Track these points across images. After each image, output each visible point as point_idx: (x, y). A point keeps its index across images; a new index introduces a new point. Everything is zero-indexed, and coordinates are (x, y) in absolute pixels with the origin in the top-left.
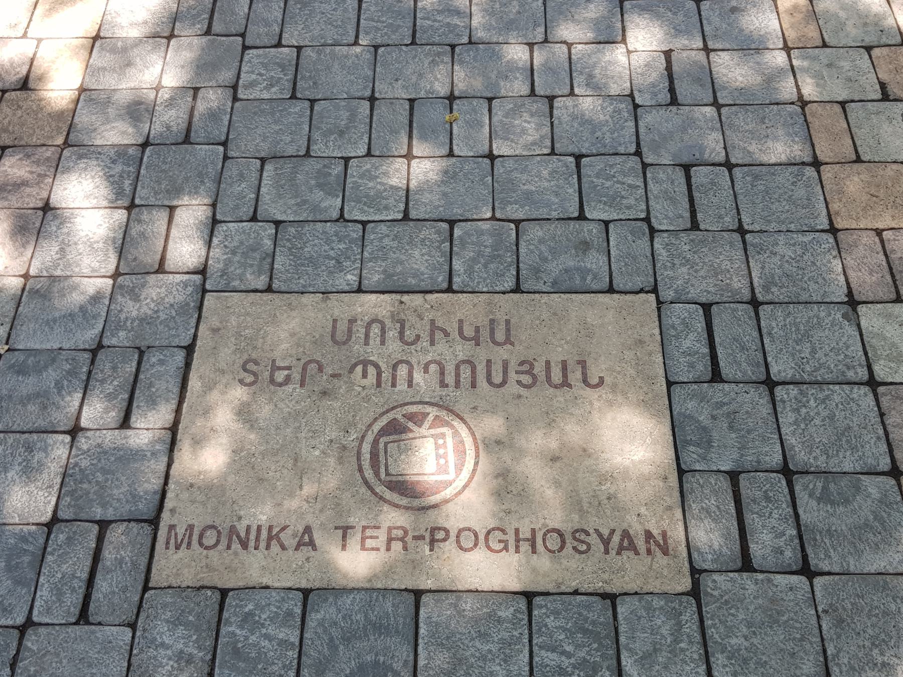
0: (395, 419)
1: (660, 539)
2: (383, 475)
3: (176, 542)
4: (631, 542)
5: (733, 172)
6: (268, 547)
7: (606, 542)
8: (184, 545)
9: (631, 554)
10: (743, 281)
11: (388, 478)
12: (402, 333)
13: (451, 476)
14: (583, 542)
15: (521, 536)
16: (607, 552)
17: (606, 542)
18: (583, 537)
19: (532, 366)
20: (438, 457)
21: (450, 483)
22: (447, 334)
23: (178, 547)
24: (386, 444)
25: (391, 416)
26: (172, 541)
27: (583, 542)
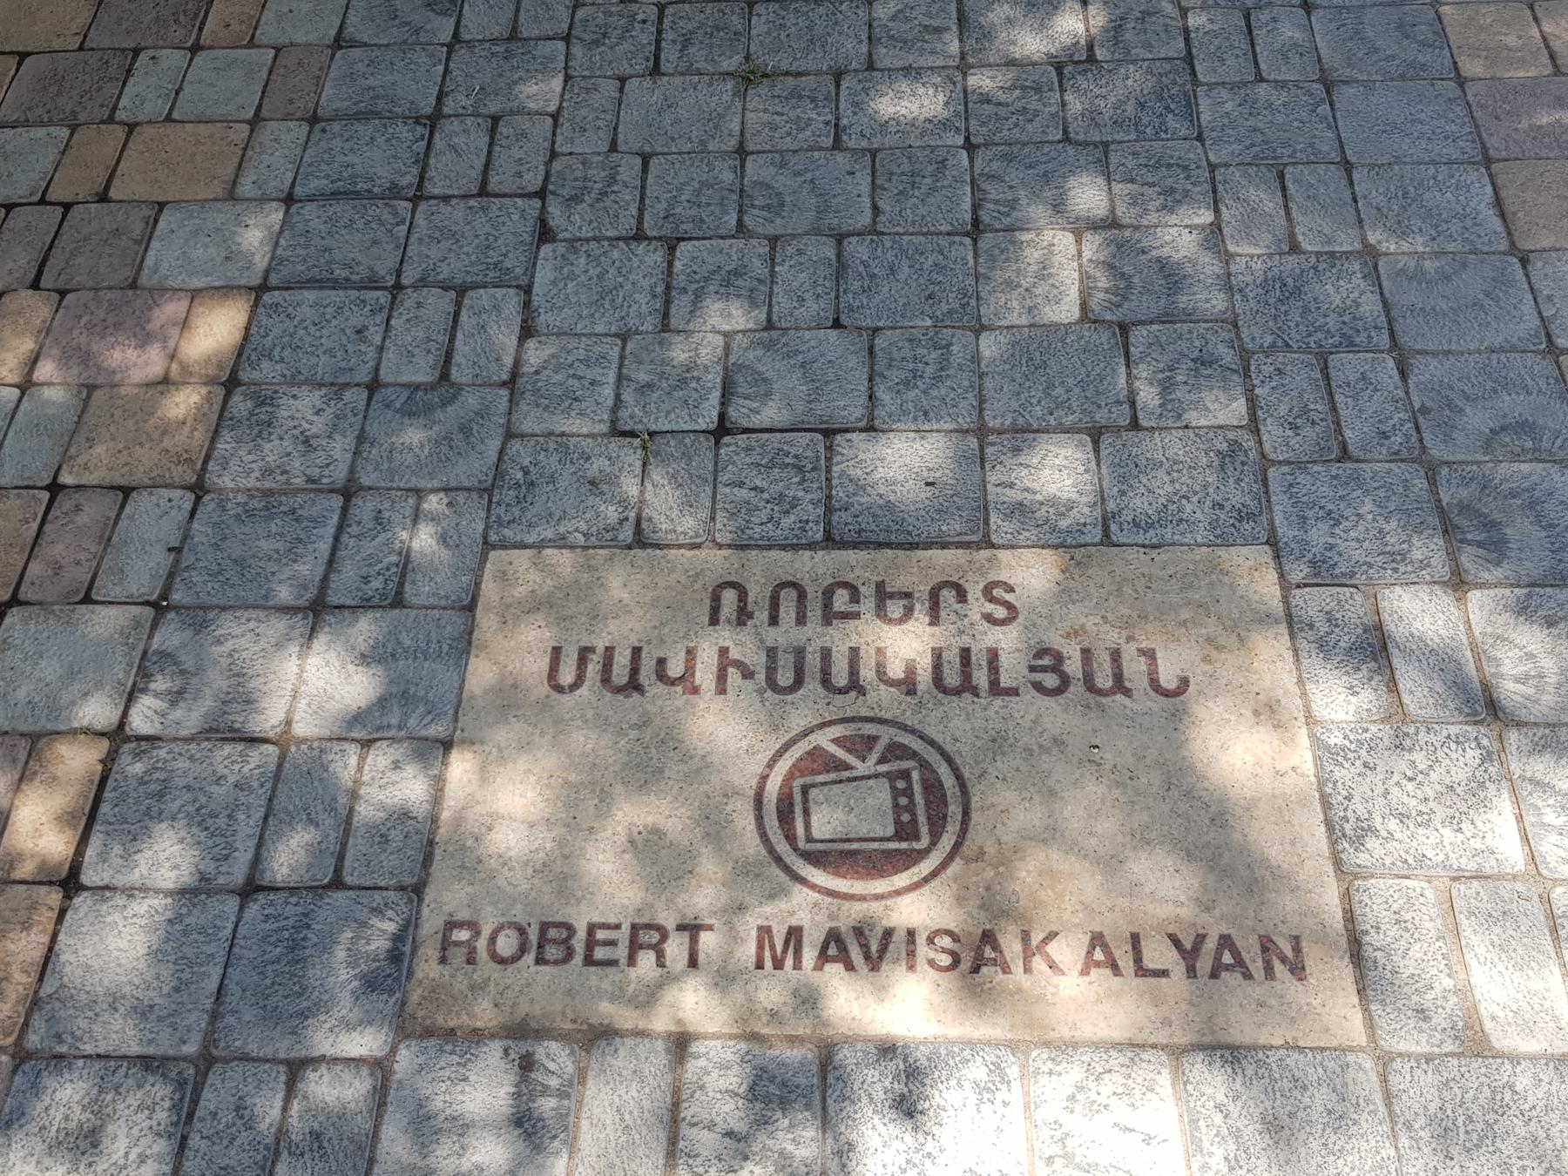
1: (1278, 966)
2: (801, 844)
3: (774, 957)
4: (1236, 954)
8: (789, 962)
11: (809, 847)
13: (924, 842)
16: (1191, 972)
19: (1059, 658)
24: (805, 790)
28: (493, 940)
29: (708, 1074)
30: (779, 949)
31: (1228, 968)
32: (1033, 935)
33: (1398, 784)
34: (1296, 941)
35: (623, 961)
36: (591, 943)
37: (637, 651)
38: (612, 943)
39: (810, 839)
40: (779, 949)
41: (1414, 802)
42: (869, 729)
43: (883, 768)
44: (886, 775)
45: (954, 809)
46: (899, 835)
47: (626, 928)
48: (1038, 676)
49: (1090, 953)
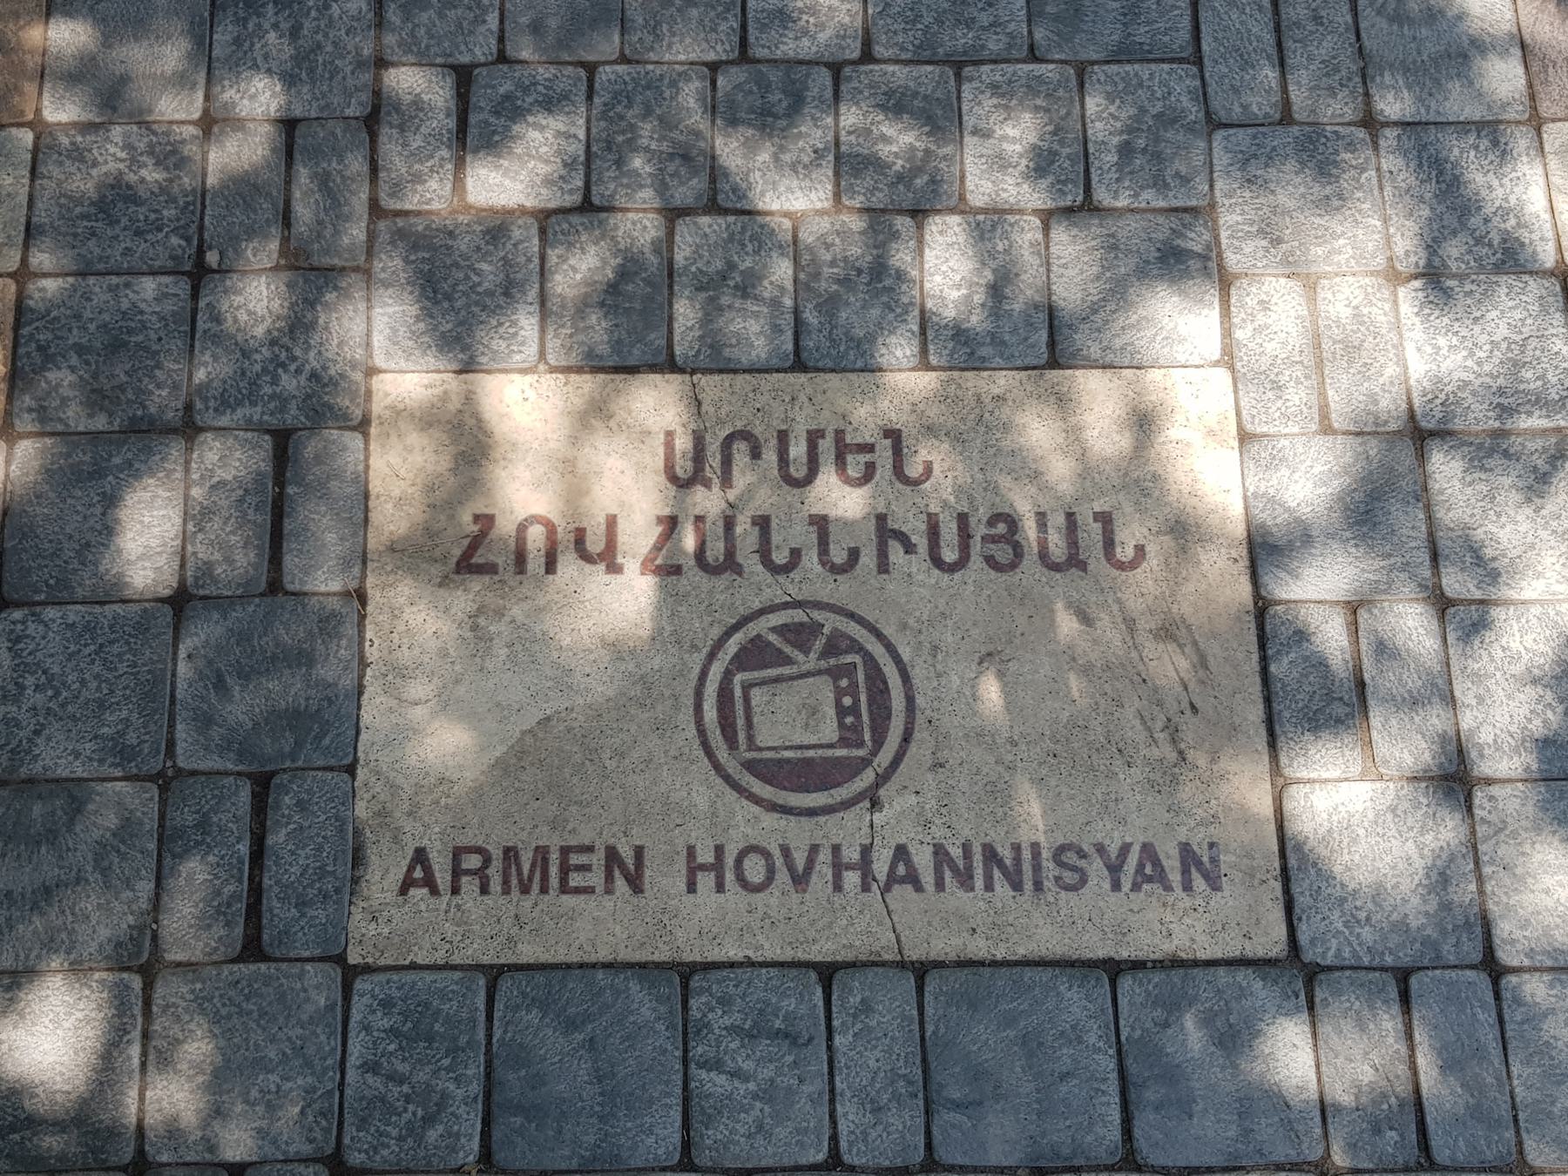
0: (759, 636)
3: (521, 881)
4: (1157, 863)
7: (1115, 869)
8: (536, 887)
9: (1156, 887)
14: (1074, 869)
15: (700, 860)
16: (1116, 886)
17: (1115, 869)
20: (841, 712)
21: (866, 763)
22: (909, 548)
23: (525, 890)
24: (747, 687)
25: (753, 629)
26: (514, 882)
27: (1074, 869)
28: (739, 862)
29: (712, 1010)
30: (526, 871)
33: (62, 706)
34: (639, 852)
35: (600, 889)
36: (565, 870)
37: (963, 519)
38: (585, 868)
40: (526, 871)
42: (798, 616)
43: (823, 664)
44: (828, 672)
45: (710, 713)
46: (843, 742)
49: (411, 869)
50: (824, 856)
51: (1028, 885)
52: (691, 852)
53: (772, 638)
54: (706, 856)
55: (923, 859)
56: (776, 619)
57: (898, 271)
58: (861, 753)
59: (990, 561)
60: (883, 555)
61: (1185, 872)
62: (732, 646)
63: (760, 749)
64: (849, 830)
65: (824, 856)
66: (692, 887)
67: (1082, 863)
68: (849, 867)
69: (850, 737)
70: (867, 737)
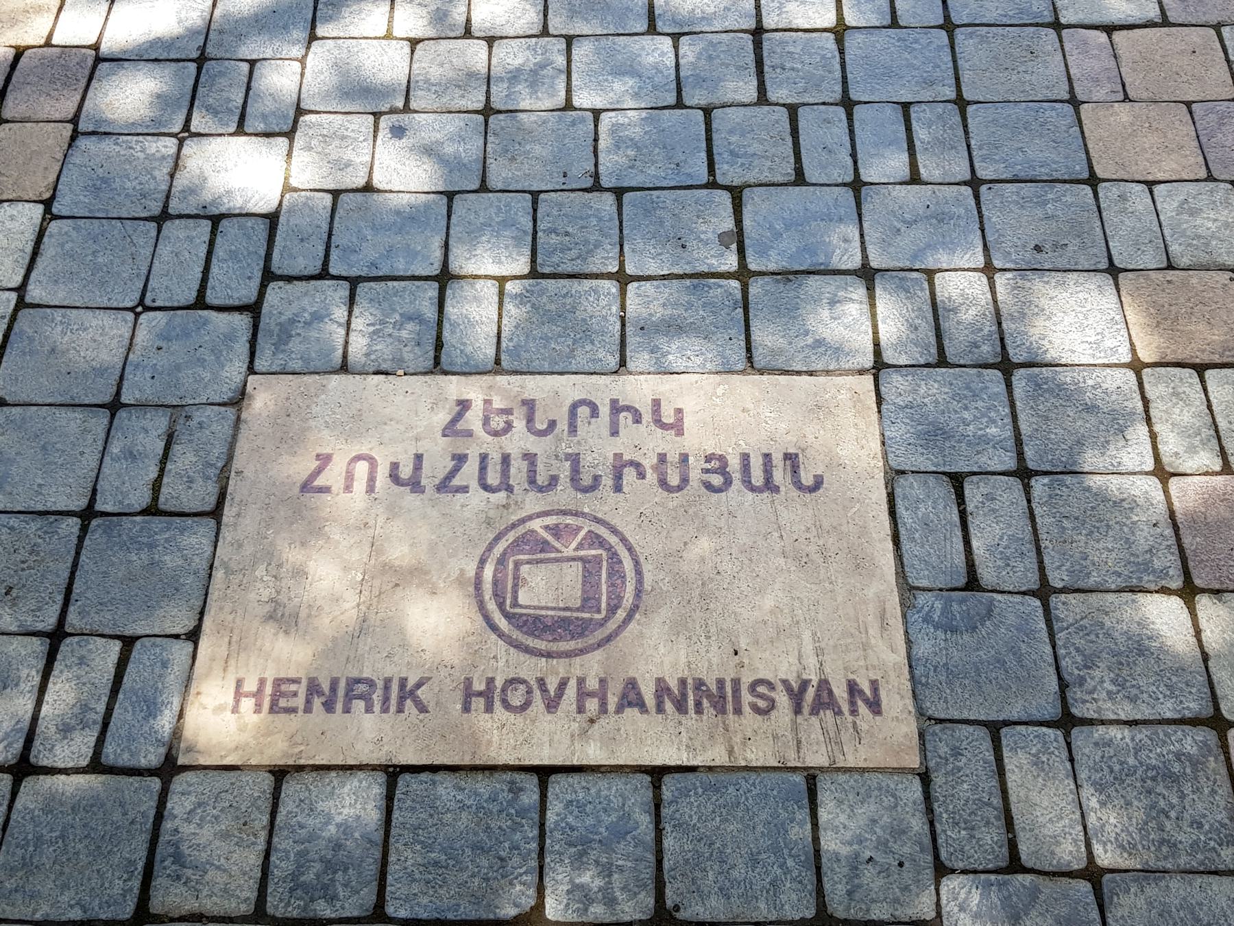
5: (279, 272)
6: (400, 710)
10: (1120, 338)
12: (530, 420)
14: (761, 696)
16: (798, 710)
18: (762, 704)
24: (517, 565)
27: (761, 696)
28: (504, 690)
31: (630, 704)
32: (548, 681)
34: (874, 684)
39: (515, 604)
41: (1160, 789)
47: (304, 682)
48: (706, 477)
50: (573, 684)
51: (730, 707)
52: (468, 682)
53: (540, 531)
54: (479, 686)
55: (648, 693)
56: (551, 520)
57: (1196, 452)
58: (597, 616)
59: (709, 486)
60: (618, 477)
61: (852, 703)
62: (511, 537)
63: (521, 607)
64: (592, 667)
65: (573, 684)
66: (466, 708)
67: (773, 694)
68: (480, 694)
69: (589, 601)
70: (604, 605)
